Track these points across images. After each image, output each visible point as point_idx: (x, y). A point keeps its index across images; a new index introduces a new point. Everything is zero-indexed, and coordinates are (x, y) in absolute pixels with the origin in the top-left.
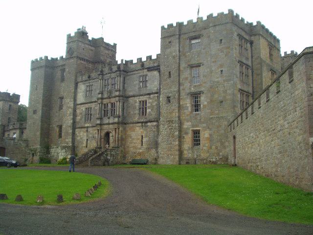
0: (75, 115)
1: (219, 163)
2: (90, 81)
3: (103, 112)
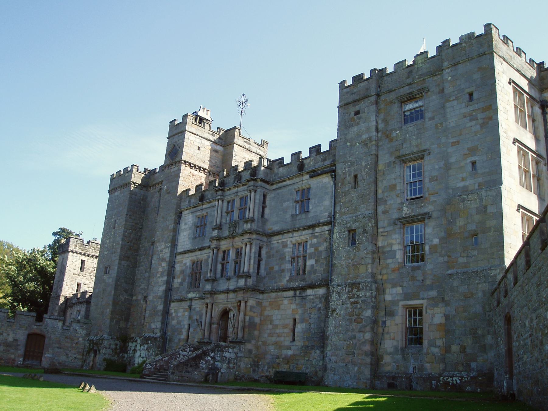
0: (171, 273)
1: (468, 389)
3: (219, 267)
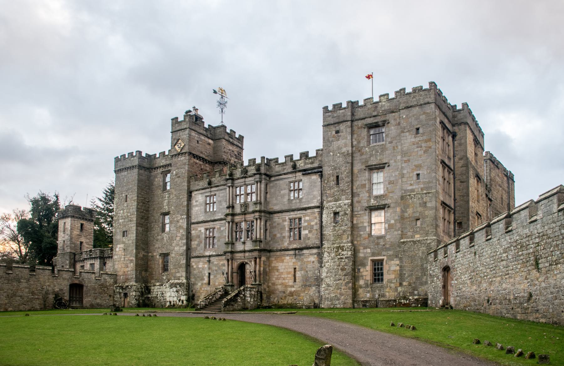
2: (213, 189)
